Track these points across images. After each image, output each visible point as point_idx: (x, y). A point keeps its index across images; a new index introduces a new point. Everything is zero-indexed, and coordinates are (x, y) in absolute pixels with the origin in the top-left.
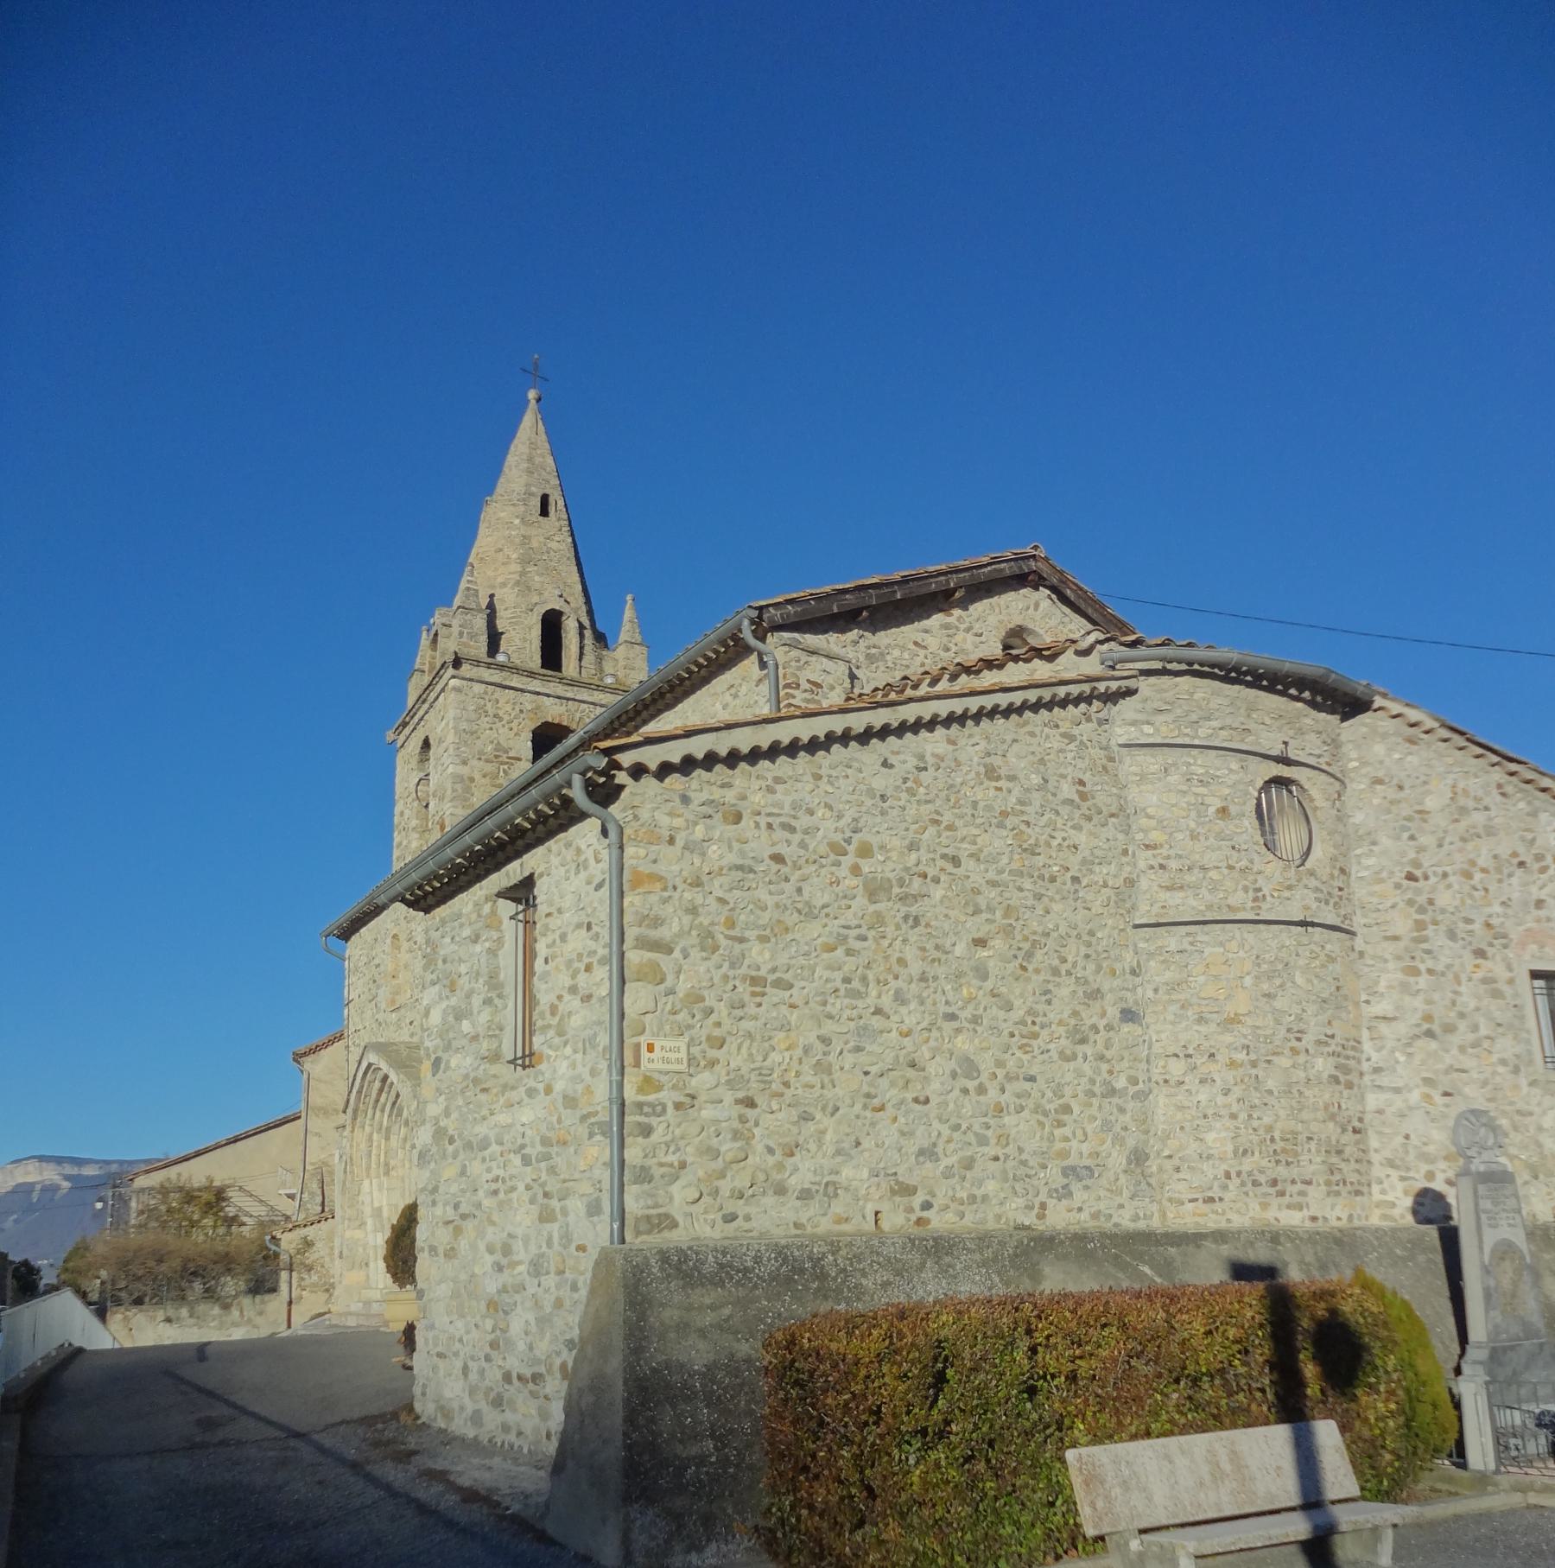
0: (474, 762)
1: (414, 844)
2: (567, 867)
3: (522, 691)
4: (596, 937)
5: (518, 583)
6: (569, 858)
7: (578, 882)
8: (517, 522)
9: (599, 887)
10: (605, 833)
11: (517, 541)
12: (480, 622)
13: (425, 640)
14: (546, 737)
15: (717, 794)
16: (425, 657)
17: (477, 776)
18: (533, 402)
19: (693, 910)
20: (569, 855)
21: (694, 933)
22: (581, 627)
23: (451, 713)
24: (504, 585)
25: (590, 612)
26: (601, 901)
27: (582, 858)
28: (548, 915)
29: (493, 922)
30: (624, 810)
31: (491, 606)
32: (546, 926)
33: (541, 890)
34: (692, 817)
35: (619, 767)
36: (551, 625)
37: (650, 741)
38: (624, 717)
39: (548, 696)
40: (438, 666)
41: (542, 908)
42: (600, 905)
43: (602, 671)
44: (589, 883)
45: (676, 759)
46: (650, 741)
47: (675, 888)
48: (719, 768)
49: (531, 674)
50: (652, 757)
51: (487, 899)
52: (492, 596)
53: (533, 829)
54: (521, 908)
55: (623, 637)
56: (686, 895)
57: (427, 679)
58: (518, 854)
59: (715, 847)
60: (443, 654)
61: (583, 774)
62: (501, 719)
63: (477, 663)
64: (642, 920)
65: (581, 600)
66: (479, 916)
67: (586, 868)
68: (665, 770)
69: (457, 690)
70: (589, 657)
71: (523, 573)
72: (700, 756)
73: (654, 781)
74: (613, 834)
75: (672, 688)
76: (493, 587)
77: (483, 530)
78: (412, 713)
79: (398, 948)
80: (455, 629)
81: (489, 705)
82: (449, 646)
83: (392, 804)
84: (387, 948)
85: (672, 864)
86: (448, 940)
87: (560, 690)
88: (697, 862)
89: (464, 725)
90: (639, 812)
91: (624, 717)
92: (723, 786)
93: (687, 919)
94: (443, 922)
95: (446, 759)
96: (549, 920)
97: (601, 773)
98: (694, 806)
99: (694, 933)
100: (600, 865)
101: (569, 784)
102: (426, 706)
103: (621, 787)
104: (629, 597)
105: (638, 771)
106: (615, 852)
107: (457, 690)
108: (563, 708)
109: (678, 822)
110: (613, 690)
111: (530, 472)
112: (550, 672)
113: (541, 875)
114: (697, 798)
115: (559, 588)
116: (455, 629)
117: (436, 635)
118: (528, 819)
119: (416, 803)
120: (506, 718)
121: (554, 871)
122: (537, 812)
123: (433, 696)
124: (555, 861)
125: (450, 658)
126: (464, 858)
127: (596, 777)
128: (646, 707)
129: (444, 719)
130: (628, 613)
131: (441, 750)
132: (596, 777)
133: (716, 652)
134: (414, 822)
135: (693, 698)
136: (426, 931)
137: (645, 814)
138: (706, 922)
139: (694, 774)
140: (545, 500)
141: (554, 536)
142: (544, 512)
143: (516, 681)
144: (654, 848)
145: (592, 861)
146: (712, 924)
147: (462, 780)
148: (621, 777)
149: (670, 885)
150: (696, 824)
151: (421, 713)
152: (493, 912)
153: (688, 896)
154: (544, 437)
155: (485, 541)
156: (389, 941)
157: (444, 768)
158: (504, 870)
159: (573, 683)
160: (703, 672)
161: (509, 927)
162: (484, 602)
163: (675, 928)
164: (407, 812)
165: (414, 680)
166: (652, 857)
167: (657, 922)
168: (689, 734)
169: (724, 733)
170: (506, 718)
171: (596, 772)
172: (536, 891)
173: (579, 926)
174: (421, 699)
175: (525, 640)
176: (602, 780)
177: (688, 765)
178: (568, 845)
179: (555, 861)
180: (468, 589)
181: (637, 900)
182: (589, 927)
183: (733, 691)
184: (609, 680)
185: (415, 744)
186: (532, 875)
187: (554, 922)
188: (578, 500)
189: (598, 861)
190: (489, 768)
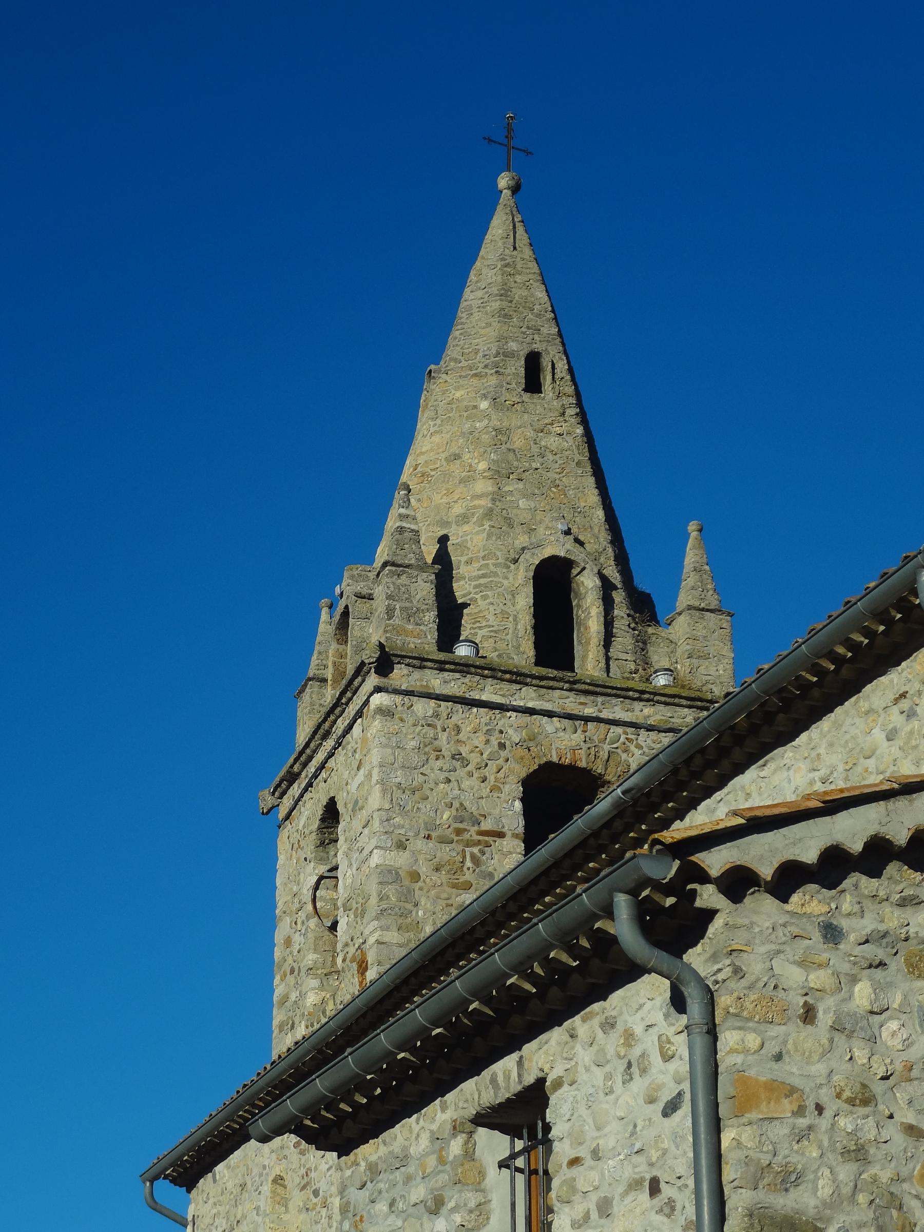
0: (419, 844)
1: (312, 999)
2: (612, 1068)
3: (503, 708)
4: (670, 1208)
5: (489, 514)
6: (611, 1050)
7: (630, 1098)
8: (484, 405)
9: (671, 1108)
10: (678, 1002)
11: (485, 438)
12: (423, 588)
13: (326, 625)
14: (553, 793)
15: (893, 919)
16: (326, 655)
17: (424, 869)
18: (507, 193)
19: (858, 1153)
20: (612, 1043)
21: (862, 1198)
22: (607, 586)
23: (375, 756)
24: (464, 519)
25: (622, 559)
26: (676, 1137)
27: (637, 1051)
28: (575, 1162)
29: (468, 1174)
30: (714, 958)
31: (443, 559)
32: (571, 1185)
33: (560, 1112)
34: (845, 967)
35: (703, 877)
36: (552, 585)
37: (759, 824)
38: (698, 760)
39: (550, 714)
40: (350, 670)
41: (562, 1150)
42: (674, 1143)
43: (647, 663)
44: (651, 1101)
45: (810, 855)
46: (759, 824)
47: (820, 1109)
48: (893, 869)
49: (518, 678)
50: (764, 854)
51: (456, 1129)
52: (443, 540)
53: (542, 995)
54: (519, 1145)
55: (684, 599)
56: (842, 1122)
57: (330, 694)
58: (514, 1044)
59: (893, 1025)
60: (359, 649)
61: (634, 892)
62: (465, 763)
63: (420, 662)
64: (758, 1175)
65: (604, 537)
66: (442, 1161)
67: (644, 1071)
68: (789, 879)
69: (386, 712)
70: (623, 641)
71: (497, 496)
72: (856, 846)
73: (768, 903)
74: (695, 1006)
75: (787, 703)
76: (447, 524)
77: (425, 424)
78: (305, 756)
79: (284, 1203)
80: (380, 604)
81: (443, 737)
82: (370, 633)
83: (271, 922)
84: (264, 1201)
85: (814, 1063)
86: (382, 1207)
87: (570, 702)
88: (861, 1055)
89: (399, 777)
90: (743, 961)
91: (698, 760)
92: (903, 903)
93: (846, 1172)
94: (374, 1170)
95: (368, 841)
96: (576, 1171)
97: (668, 889)
98: (848, 944)
99: (862, 1198)
100: (673, 1066)
101: (609, 912)
102: (329, 744)
103: (709, 915)
104: (692, 527)
105: (738, 883)
106: (700, 1041)
107: (386, 712)
108: (578, 737)
109: (818, 979)
110: (669, 698)
111: (504, 316)
112: (552, 673)
113: (558, 1084)
114: (856, 928)
115: (564, 517)
116: (380, 604)
117: (346, 613)
118: (532, 978)
119: (313, 922)
120: (475, 759)
121: (582, 1076)
122: (547, 963)
123: (341, 724)
124: (584, 1056)
125: (370, 655)
126: (413, 1050)
127: (657, 897)
128: (739, 740)
129: (362, 769)
130: (692, 556)
131: (357, 824)
132: (657, 897)
133: (868, 633)
134: (311, 958)
135: (826, 723)
136: (342, 1191)
137: (755, 966)
138: (885, 1176)
139: (847, 883)
140: (533, 362)
141: (550, 427)
142: (533, 384)
143: (490, 692)
144: (774, 1031)
145: (655, 1058)
146: (898, 1179)
147: (398, 878)
148: (708, 896)
149: (810, 1104)
150: (854, 980)
151: (320, 757)
152: (469, 1154)
153: (846, 1123)
154: (527, 252)
155: (429, 444)
156: (266, 1188)
157: (364, 854)
158: (486, 1074)
159: (595, 689)
160: (845, 671)
161: (498, 1183)
162: (430, 551)
163: (825, 1189)
164: (297, 938)
165: (306, 696)
166: (772, 1048)
167: (789, 1179)
168: (834, 806)
169: (901, 803)
170: (475, 759)
171: (657, 886)
172: (549, 1116)
173: (635, 1185)
174: (321, 732)
175: (505, 615)
176: (670, 901)
177: (833, 867)
178: (609, 1025)
179: (584, 1056)
180: (401, 530)
181: (747, 1136)
182: (654, 1188)
183: (905, 704)
184: (661, 681)
185: (310, 813)
186: (541, 1081)
187: (585, 1177)
188: (587, 367)
189: (667, 1058)
190: (446, 853)
